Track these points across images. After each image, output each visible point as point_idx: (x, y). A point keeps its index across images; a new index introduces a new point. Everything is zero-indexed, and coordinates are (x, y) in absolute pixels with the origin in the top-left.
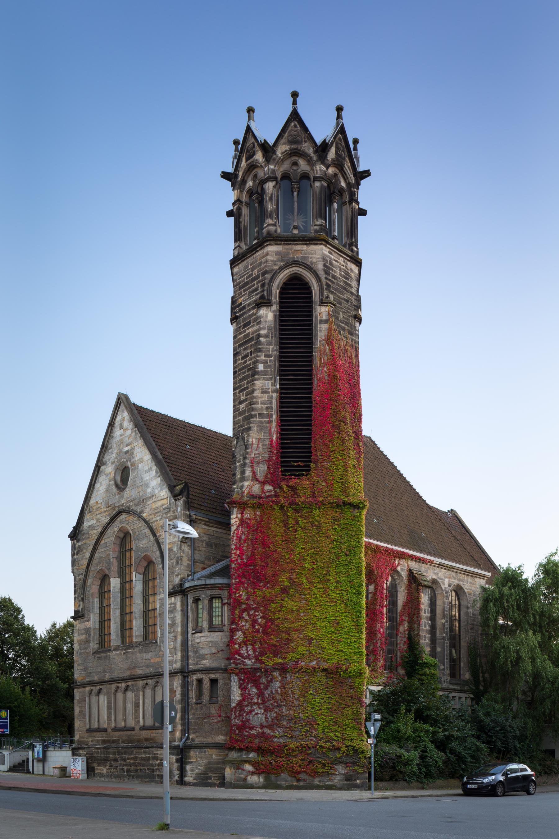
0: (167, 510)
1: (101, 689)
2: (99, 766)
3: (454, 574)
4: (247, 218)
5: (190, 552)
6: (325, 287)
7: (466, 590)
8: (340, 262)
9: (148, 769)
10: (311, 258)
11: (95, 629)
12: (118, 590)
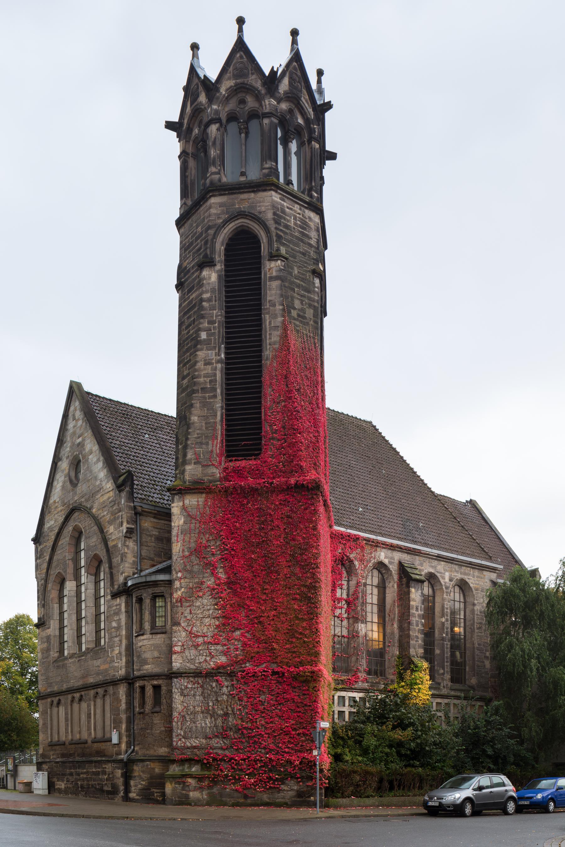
0: (113, 503)
1: (60, 700)
2: (58, 781)
3: (456, 567)
4: (193, 172)
5: (136, 548)
6: (275, 238)
7: (471, 585)
8: (294, 212)
9: (98, 784)
10: (259, 206)
11: (55, 636)
12: (73, 593)
